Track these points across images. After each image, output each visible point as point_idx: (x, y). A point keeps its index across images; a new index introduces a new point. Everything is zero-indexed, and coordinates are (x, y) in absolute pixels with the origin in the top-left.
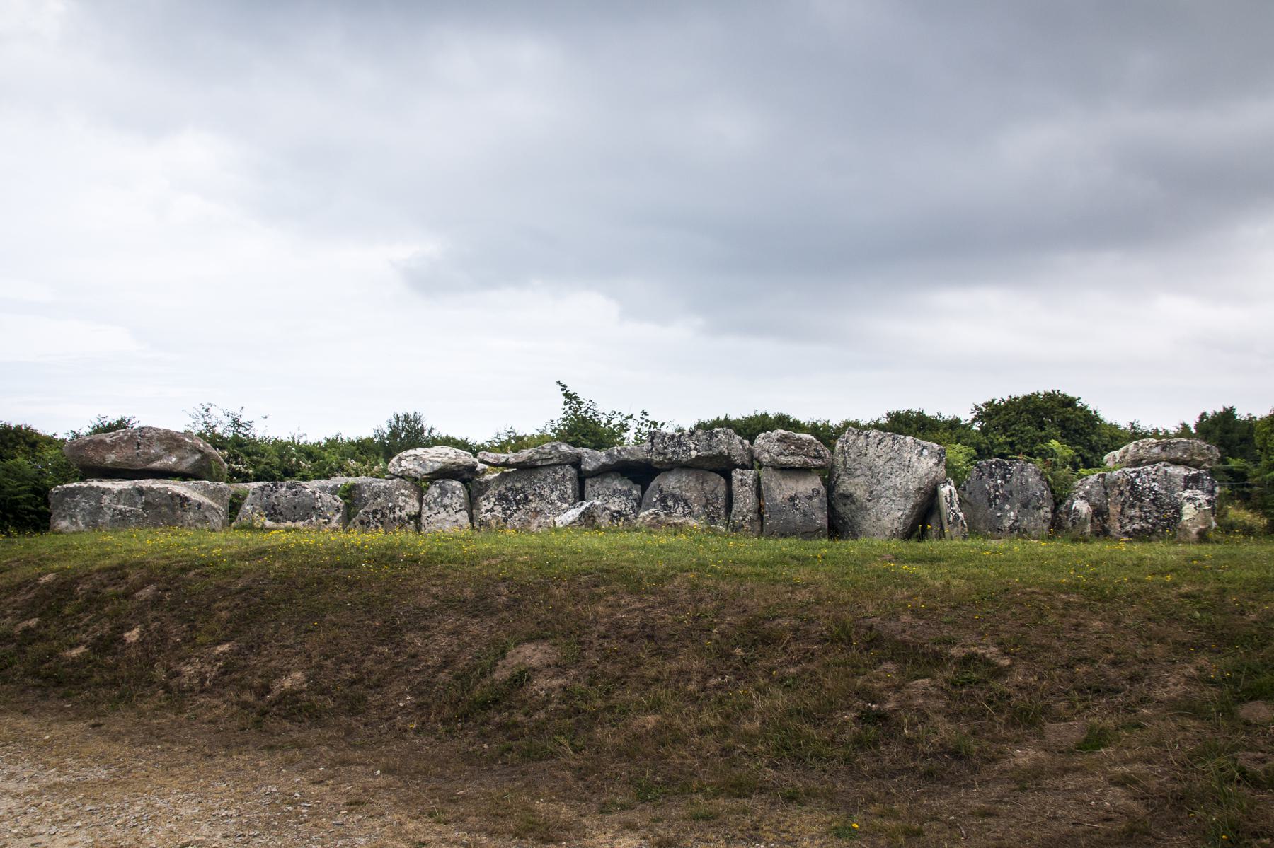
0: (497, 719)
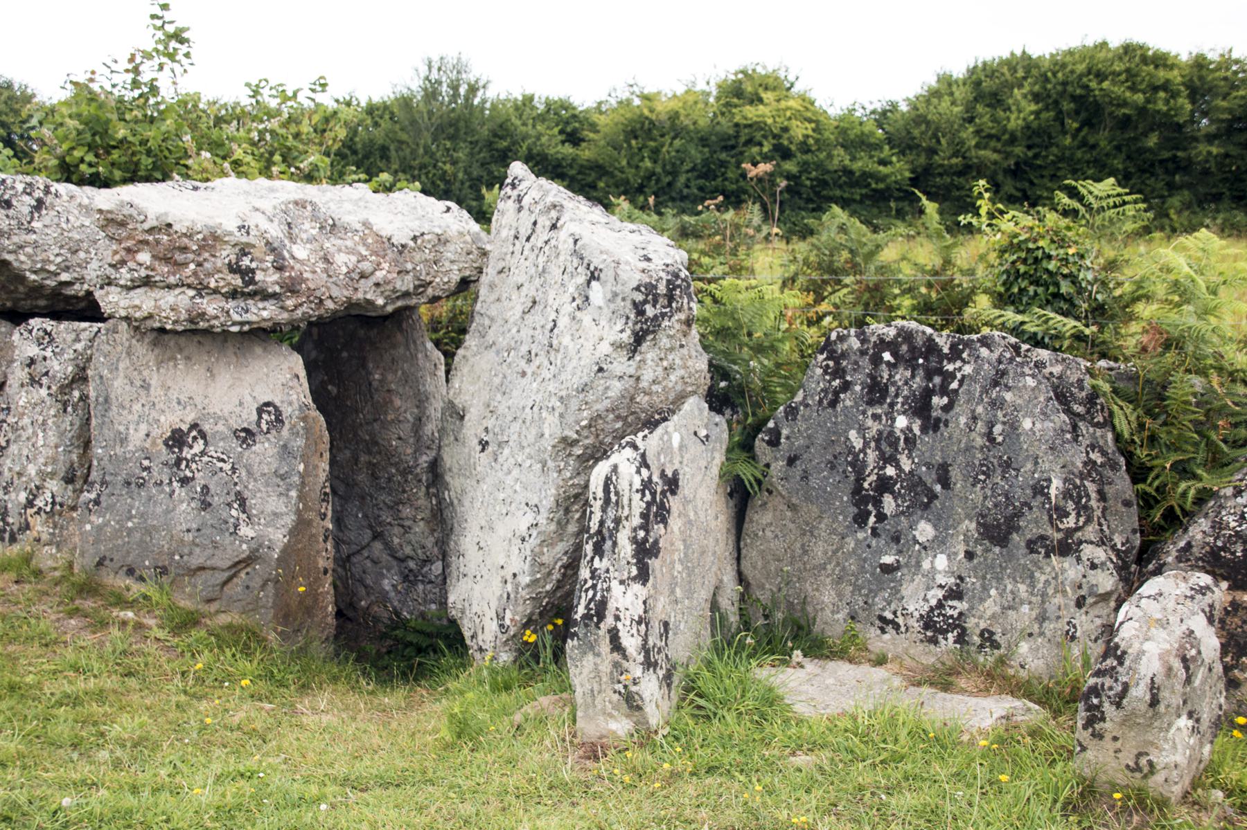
0: (874, 186)
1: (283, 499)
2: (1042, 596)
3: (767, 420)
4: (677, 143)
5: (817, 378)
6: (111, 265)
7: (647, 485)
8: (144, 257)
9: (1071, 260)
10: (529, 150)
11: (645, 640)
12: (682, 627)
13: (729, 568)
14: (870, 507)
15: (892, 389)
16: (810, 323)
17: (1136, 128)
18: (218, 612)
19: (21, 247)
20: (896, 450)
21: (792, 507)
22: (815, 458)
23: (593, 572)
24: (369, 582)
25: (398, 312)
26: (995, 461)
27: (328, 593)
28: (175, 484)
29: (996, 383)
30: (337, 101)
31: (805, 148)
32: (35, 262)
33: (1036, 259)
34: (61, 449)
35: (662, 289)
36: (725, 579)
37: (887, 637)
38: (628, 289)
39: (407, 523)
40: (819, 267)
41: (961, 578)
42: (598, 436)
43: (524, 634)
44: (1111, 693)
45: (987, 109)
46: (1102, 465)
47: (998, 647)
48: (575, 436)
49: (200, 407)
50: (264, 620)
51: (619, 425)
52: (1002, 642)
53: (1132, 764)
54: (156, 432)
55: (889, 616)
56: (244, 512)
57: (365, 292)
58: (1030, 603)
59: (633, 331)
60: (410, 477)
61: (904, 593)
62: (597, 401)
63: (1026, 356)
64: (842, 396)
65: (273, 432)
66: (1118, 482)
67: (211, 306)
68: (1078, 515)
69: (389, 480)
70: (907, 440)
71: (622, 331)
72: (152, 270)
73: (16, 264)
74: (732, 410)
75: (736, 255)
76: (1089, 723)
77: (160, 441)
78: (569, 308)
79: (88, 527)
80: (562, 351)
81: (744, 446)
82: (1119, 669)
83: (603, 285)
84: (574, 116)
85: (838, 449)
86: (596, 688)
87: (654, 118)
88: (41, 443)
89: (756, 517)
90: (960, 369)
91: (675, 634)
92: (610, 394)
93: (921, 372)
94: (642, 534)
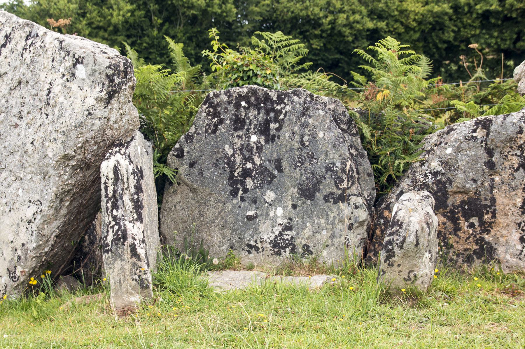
2: (332, 224)
3: (175, 143)
5: (202, 118)
9: (269, 77)
14: (239, 186)
15: (247, 121)
17: (201, 24)
20: (252, 154)
21: (193, 190)
22: (206, 162)
26: (305, 155)
29: (303, 114)
33: (249, 77)
35: (122, 68)
38: (103, 68)
41: (291, 219)
42: (85, 153)
44: (398, 242)
45: (95, 7)
46: (356, 156)
47: (312, 253)
48: (73, 153)
52: (313, 251)
53: (406, 277)
55: (253, 243)
58: (327, 229)
59: (107, 92)
61: (260, 230)
63: (316, 100)
64: (219, 127)
66: (364, 164)
68: (348, 181)
70: (257, 148)
71: (101, 91)
76: (387, 259)
80: (59, 105)
82: (400, 230)
83: (86, 66)
85: (219, 156)
86: (122, 278)
89: (170, 199)
90: (284, 108)
92: (94, 128)
93: (263, 111)
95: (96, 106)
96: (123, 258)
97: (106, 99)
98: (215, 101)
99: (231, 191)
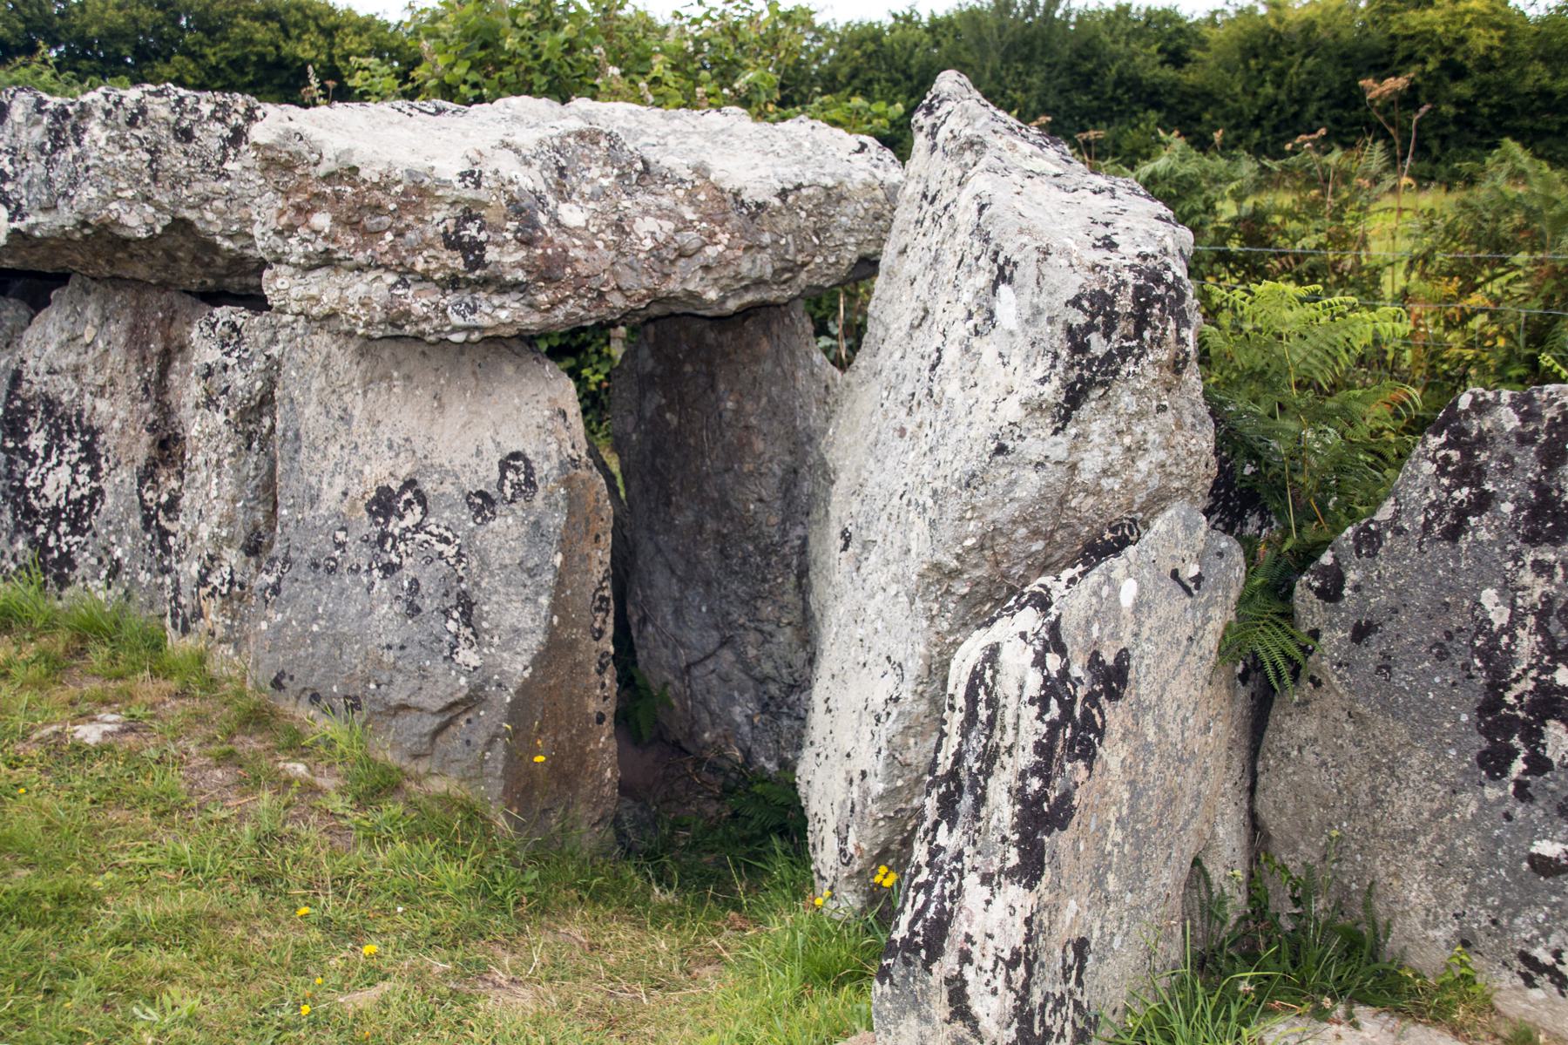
1: (530, 607)
4: (1310, 62)
6: (278, 233)
7: (1054, 687)
8: (322, 220)
10: (1120, 73)
11: (1023, 997)
12: (1116, 944)
13: (1230, 810)
14: (1516, 741)
16: (1450, 325)
18: (429, 774)
19: (207, 200)
22: (1408, 634)
23: (935, 852)
24: (714, 706)
25: (747, 312)
27: (604, 751)
28: (376, 572)
30: (895, 16)
31: (1486, 64)
32: (231, 223)
34: (240, 505)
35: (1124, 303)
36: (1220, 831)
37: (1536, 994)
39: (768, 628)
40: (1474, 238)
42: (997, 564)
43: (874, 873)
48: (954, 564)
49: (419, 454)
50: (490, 793)
51: (1038, 545)
54: (356, 491)
55: (1546, 958)
56: (468, 625)
57: (684, 280)
60: (774, 558)
62: (994, 505)
64: (1472, 520)
65: (521, 500)
67: (419, 301)
69: (745, 561)
71: (1044, 380)
72: (334, 241)
73: (200, 225)
74: (1262, 518)
75: (1340, 219)
77: (361, 504)
78: (961, 330)
79: (264, 625)
81: (1271, 594)
83: (1018, 292)
84: (1180, 31)
85: (1457, 622)
87: (1282, 30)
88: (214, 494)
89: (1288, 723)
91: (1100, 960)
92: (1019, 493)
94: (1035, 784)
95: (1026, 425)
96: (924, 1012)
97: (1057, 405)
98: (1475, 425)
99: (1484, 753)
